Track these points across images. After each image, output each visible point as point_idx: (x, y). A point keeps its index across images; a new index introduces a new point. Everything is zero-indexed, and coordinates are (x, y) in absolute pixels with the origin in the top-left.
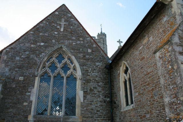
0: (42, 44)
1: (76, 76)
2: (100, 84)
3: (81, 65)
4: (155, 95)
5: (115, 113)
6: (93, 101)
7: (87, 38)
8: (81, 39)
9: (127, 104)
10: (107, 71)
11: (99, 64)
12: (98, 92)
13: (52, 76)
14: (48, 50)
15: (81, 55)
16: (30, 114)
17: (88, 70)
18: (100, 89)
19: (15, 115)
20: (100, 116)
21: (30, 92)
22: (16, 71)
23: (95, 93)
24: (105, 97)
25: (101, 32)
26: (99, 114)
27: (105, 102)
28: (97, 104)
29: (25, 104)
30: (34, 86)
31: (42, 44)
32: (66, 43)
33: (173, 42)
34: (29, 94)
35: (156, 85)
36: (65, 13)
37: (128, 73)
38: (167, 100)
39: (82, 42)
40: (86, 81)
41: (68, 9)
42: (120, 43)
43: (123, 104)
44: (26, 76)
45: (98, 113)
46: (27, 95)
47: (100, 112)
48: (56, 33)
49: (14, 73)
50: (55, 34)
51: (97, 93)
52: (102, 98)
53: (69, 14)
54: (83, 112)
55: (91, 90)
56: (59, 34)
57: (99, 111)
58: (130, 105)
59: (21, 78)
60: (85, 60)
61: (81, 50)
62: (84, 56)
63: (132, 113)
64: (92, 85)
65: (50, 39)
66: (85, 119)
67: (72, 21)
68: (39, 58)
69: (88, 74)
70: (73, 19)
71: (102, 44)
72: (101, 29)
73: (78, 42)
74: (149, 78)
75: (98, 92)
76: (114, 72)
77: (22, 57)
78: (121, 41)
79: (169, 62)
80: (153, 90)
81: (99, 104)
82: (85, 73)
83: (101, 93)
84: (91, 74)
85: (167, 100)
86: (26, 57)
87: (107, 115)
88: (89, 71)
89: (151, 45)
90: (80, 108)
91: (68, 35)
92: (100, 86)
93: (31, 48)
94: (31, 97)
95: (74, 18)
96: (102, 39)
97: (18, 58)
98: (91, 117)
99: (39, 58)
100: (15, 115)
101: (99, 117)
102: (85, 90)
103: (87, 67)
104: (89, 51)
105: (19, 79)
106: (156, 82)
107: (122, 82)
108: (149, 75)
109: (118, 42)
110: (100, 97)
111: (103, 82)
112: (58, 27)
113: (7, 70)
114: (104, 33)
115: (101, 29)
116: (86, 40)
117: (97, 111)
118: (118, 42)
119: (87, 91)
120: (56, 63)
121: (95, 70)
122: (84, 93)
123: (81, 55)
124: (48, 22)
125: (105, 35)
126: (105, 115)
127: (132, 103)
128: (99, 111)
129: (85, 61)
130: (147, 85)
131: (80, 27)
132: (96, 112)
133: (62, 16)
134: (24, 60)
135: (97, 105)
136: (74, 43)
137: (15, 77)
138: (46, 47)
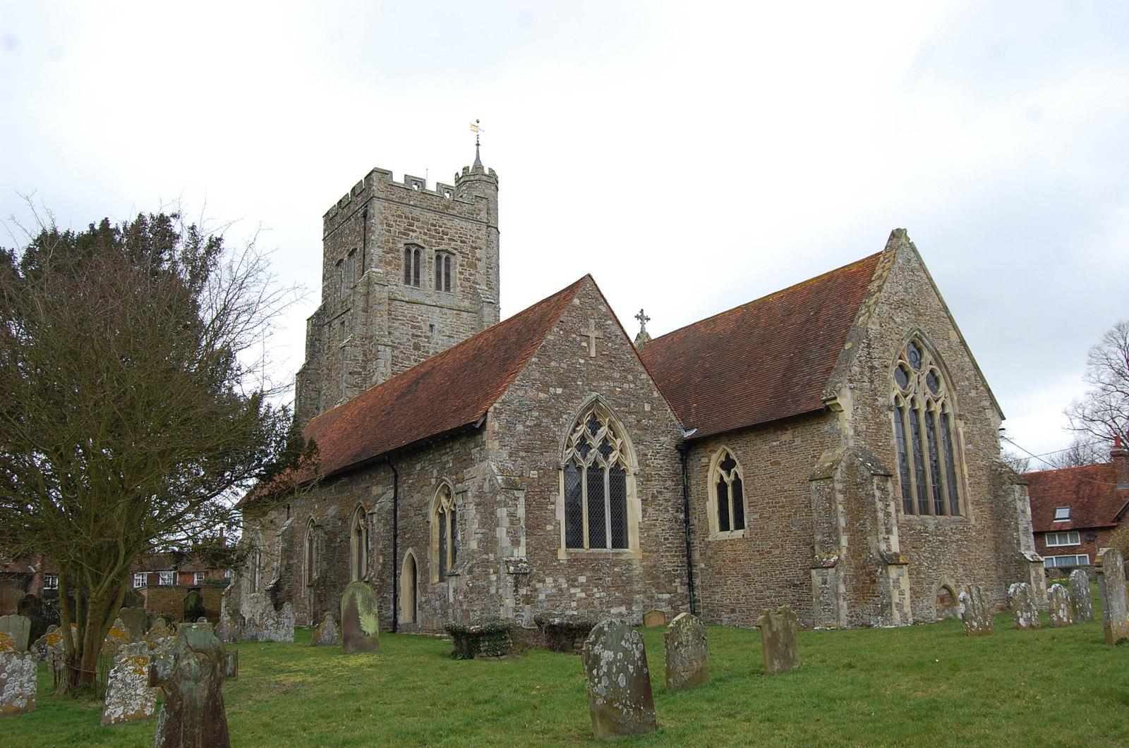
9: (724, 526)
50: (580, 364)
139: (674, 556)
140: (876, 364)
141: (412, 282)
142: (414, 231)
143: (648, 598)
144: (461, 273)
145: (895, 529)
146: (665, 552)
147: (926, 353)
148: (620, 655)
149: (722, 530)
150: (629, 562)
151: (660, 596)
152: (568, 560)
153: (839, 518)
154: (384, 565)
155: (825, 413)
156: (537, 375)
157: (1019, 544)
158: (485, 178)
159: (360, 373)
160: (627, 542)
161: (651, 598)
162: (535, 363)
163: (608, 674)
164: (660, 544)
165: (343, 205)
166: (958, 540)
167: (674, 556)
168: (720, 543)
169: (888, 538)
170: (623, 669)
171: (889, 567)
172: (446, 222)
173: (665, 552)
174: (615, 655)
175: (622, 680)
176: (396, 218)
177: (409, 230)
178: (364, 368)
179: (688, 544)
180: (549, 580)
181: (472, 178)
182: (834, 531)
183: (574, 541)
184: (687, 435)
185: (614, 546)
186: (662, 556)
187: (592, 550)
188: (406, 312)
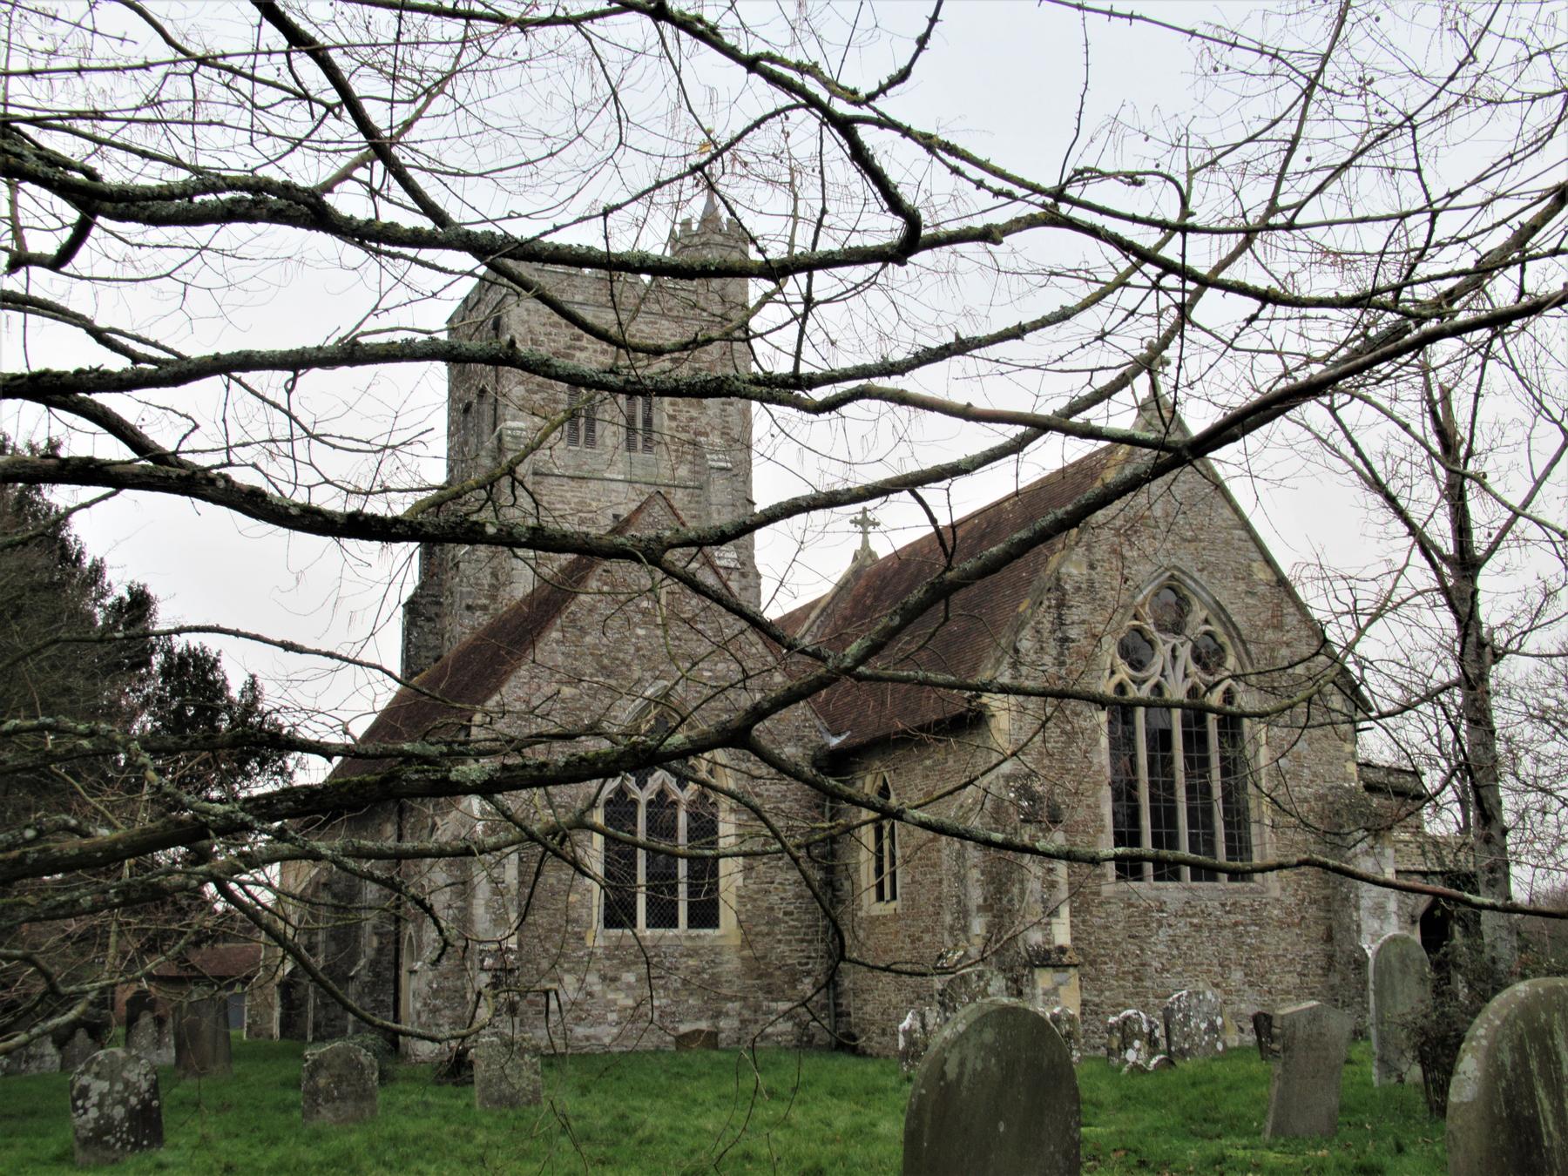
9: (880, 897)
28: (785, 891)
42: (865, 533)
50: (638, 637)
117: (786, 914)
139: (802, 941)
140: (1073, 633)
141: (582, 440)
142: (582, 349)
143: (748, 1008)
144: (672, 418)
145: (1065, 911)
146: (785, 934)
147: (1196, 605)
148: (119, 1087)
149: (610, 922)
150: (716, 951)
151: (774, 1005)
152: (606, 948)
153: (970, 889)
154: (380, 951)
155: (972, 722)
156: (560, 659)
157: (1359, 931)
158: (719, 239)
159: (485, 608)
160: (717, 918)
161: (756, 1009)
162: (557, 642)
163: (100, 1105)
164: (776, 922)
165: (471, 304)
166: (1236, 924)
167: (802, 941)
168: (874, 920)
169: (1049, 924)
170: (124, 1102)
171: (1037, 971)
172: (643, 327)
173: (785, 934)
174: (112, 1085)
175: (119, 1112)
176: (549, 329)
177: (574, 348)
178: (493, 598)
179: (834, 922)
180: (569, 979)
181: (696, 240)
182: (963, 913)
183: (618, 913)
184: (835, 742)
185: (693, 923)
186: (779, 941)
187: (694, 932)
188: (568, 495)
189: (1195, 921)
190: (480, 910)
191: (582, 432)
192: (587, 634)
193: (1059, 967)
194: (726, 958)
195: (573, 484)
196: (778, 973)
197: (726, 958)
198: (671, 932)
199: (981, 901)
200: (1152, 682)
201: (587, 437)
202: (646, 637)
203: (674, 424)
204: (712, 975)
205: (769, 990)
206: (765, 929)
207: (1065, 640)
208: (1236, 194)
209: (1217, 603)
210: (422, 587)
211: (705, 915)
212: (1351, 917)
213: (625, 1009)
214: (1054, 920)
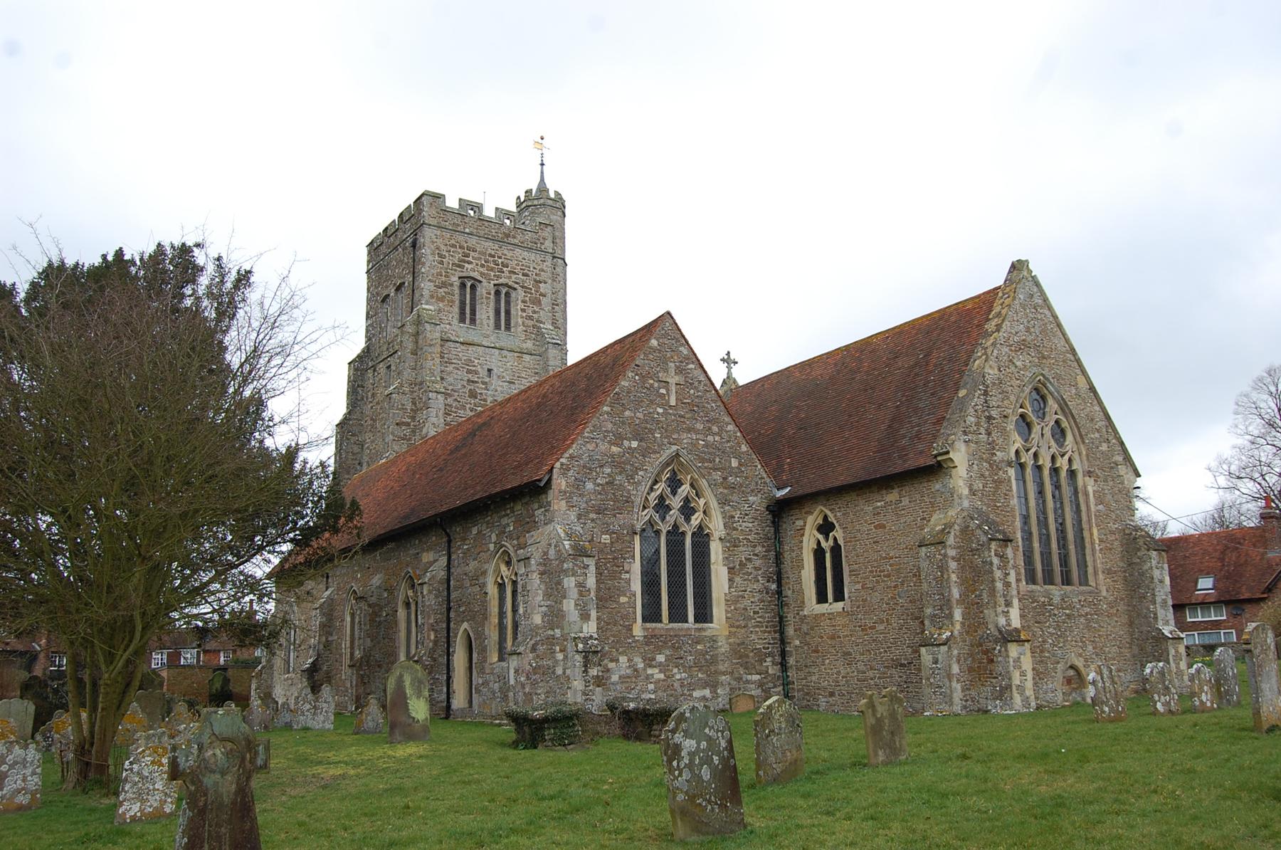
0: (635, 444)
1: (709, 529)
2: (759, 549)
3: (723, 502)
4: (900, 597)
5: (786, 617)
6: (746, 591)
7: (728, 424)
8: (715, 429)
9: (822, 598)
10: (770, 517)
11: (755, 498)
12: (755, 568)
13: (663, 530)
14: (649, 462)
15: (717, 476)
16: (636, 622)
17: (734, 513)
18: (758, 563)
19: (608, 624)
20: (759, 625)
21: (627, 572)
22: (593, 520)
23: (749, 571)
24: (768, 581)
25: (542, 188)
26: (758, 619)
27: (767, 593)
28: (753, 597)
29: (623, 599)
30: (633, 557)
31: (635, 444)
32: (685, 441)
33: (948, 543)
34: (627, 576)
35: (903, 581)
36: (674, 342)
37: (831, 534)
38: (929, 611)
39: (717, 438)
40: (731, 544)
41: (680, 330)
42: (729, 368)
43: (810, 599)
44: (615, 533)
45: (756, 616)
46: (623, 579)
47: (760, 615)
48: (660, 410)
49: (590, 524)
50: (658, 414)
51: (753, 571)
52: (763, 584)
53: (682, 345)
54: (729, 615)
55: (741, 564)
56: (666, 413)
57: (758, 613)
58: (831, 604)
59: (606, 538)
60: (726, 488)
61: (717, 460)
62: (725, 479)
63: (840, 621)
64: (743, 553)
65: (650, 430)
66: (733, 630)
67: (691, 369)
68: (633, 483)
69: (735, 525)
70: (693, 363)
71: (549, 258)
72: (542, 164)
73: (710, 438)
74: (890, 565)
75: (755, 568)
76: (785, 520)
77: (599, 481)
78: (732, 357)
79: (938, 567)
80: (896, 586)
81: (758, 596)
82: (729, 523)
83: (760, 572)
84: (740, 526)
85: (929, 611)
86: (606, 483)
87: (772, 621)
88: (736, 519)
89: (903, 512)
90: (723, 607)
91: (687, 416)
92: (758, 556)
93: (612, 456)
94: (632, 584)
95: (697, 362)
96: (549, 228)
97: (590, 486)
98: (744, 627)
99: (633, 483)
100: (608, 624)
101: (757, 626)
102: (731, 565)
103: (732, 506)
104: (734, 463)
105: (602, 541)
106: (905, 577)
107: (810, 550)
108: (891, 561)
109: (723, 360)
110: (758, 581)
111: (763, 546)
112: (663, 391)
113: (573, 517)
114: (557, 193)
115: (542, 164)
116: (727, 432)
117: (754, 613)
118: (723, 360)
119: (733, 568)
120: (667, 496)
121: (747, 515)
122: (729, 573)
123: (717, 476)
124: (637, 375)
125: (558, 204)
126: (768, 622)
127: (839, 596)
128: (758, 613)
129: (726, 491)
130: (885, 576)
131: (710, 391)
132: (752, 614)
133: (669, 355)
134: (603, 489)
135: (752, 600)
136: (701, 442)
137: (593, 537)
138: (645, 452)
139: (765, 632)
140: (994, 413)
150: (713, 640)
152: (645, 637)
154: (435, 642)
155: (936, 469)
157: (1156, 618)
166: (1087, 614)
167: (765, 632)
168: (818, 617)
169: (1008, 612)
170: (708, 761)
171: (1009, 645)
174: (698, 743)
175: (706, 773)
177: (465, 262)
178: (413, 418)
179: (781, 618)
180: (623, 659)
181: (536, 202)
183: (651, 615)
184: (780, 494)
185: (697, 621)
187: (697, 625)
189: (1067, 611)
190: (569, 606)
191: (468, 316)
192: (626, 409)
193: (1020, 641)
194: (720, 644)
195: (463, 347)
196: (751, 654)
197: (720, 644)
198: (659, 625)
199: (958, 596)
200: (1033, 450)
201: (471, 319)
202: (662, 414)
203: (524, 314)
204: (712, 656)
205: (746, 666)
206: (742, 623)
207: (989, 418)
208: (290, 382)
209: (1063, 399)
210: (349, 413)
211: (704, 615)
212: (1148, 609)
213: (659, 680)
214: (1011, 610)
